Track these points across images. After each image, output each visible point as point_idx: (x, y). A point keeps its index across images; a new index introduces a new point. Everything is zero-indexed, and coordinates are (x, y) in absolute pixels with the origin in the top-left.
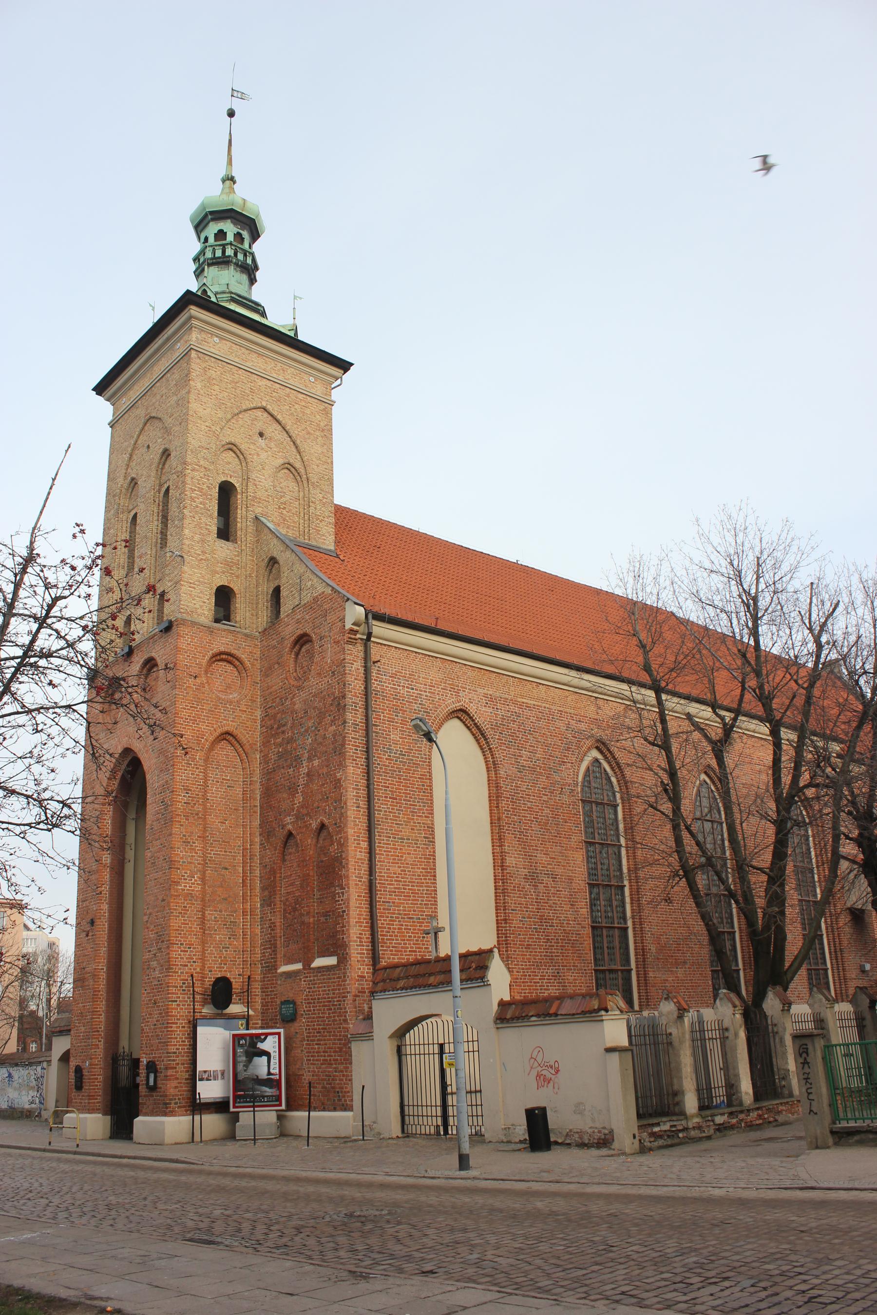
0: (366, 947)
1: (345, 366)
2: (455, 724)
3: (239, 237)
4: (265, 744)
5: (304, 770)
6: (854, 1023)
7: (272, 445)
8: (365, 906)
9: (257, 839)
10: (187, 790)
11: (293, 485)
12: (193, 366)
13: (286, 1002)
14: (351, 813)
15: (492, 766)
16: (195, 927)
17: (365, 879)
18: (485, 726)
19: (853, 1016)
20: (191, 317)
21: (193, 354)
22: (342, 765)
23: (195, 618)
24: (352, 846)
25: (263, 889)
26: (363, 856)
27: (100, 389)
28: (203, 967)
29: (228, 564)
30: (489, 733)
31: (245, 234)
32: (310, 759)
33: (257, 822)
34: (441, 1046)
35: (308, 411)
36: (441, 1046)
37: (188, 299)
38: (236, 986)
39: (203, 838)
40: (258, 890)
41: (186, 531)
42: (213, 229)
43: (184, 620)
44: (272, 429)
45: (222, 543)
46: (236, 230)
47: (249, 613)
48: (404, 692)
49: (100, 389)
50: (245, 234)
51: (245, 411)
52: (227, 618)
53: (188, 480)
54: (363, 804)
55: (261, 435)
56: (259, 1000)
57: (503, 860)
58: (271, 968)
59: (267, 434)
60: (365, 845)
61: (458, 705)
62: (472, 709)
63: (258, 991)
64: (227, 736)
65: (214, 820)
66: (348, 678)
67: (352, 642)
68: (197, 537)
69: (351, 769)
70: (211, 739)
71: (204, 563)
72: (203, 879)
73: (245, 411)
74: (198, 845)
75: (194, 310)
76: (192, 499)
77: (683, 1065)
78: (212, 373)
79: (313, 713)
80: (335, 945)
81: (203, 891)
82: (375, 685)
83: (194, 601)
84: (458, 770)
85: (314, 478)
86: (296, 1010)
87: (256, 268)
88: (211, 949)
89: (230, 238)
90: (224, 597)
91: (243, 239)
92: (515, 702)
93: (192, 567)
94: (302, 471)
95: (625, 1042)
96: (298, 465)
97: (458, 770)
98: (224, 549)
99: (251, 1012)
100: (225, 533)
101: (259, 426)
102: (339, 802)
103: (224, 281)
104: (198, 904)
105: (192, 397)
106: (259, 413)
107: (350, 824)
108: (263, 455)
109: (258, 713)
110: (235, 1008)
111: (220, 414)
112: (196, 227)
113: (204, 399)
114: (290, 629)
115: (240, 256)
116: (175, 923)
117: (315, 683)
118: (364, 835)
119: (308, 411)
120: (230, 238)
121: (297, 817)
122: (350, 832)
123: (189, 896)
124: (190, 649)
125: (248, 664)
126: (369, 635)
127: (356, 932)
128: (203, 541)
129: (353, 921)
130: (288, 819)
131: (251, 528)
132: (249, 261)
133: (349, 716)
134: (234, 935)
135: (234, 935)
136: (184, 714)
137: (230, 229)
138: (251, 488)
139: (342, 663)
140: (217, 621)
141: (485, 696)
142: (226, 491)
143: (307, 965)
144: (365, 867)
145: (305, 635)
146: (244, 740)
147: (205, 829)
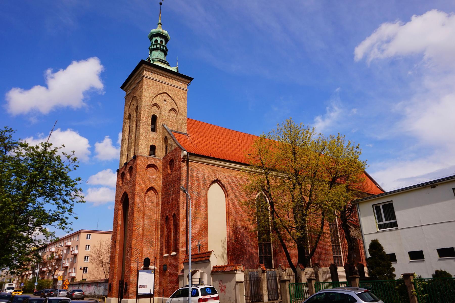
0: (184, 250)
1: (191, 79)
2: (216, 185)
3: (161, 41)
4: (163, 190)
5: (171, 198)
6: (345, 274)
7: (168, 103)
8: (184, 238)
9: (160, 218)
10: (139, 204)
11: (174, 115)
12: (144, 81)
13: (164, 265)
14: (181, 210)
15: (227, 195)
16: (140, 243)
17: (185, 230)
18: (225, 184)
19: (345, 272)
20: (144, 67)
21: (144, 78)
22: (179, 197)
23: (143, 155)
24: (181, 220)
25: (161, 232)
26: (185, 223)
27: (122, 87)
28: (142, 255)
29: (154, 139)
30: (226, 186)
31: (163, 40)
32: (172, 195)
33: (160, 213)
34: (200, 279)
35: (179, 93)
36: (200, 279)
37: (142, 62)
38: (152, 260)
39: (143, 217)
40: (159, 232)
41: (141, 130)
42: (154, 39)
43: (139, 155)
44: (169, 99)
45: (152, 132)
46: (160, 39)
47: (160, 153)
48: (199, 175)
49: (122, 87)
50: (163, 40)
51: (160, 94)
52: (154, 154)
53: (142, 115)
54: (185, 208)
55: (165, 101)
56: (159, 264)
57: (229, 223)
58: (162, 254)
59: (167, 100)
60: (185, 220)
61: (216, 179)
62: (221, 179)
63: (158, 262)
64: (152, 188)
65: (147, 212)
66: (182, 172)
67: (184, 162)
68: (144, 131)
69: (181, 198)
70: (147, 189)
71: (146, 139)
72: (143, 229)
73: (160, 94)
74: (142, 220)
75: (144, 65)
76: (143, 120)
77: (96, 279)
78: (150, 83)
79: (173, 182)
80: (176, 249)
81: (143, 233)
82: (190, 173)
83: (144, 150)
84: (216, 198)
85: (181, 112)
86: (167, 267)
87: (167, 50)
88: (145, 250)
89: (159, 42)
90: (153, 149)
91: (163, 42)
92: (235, 177)
93: (142, 140)
94: (177, 111)
95: (346, 281)
96: (176, 109)
97: (216, 198)
98: (153, 134)
99: (156, 268)
100: (154, 129)
101: (164, 98)
102: (178, 207)
103: (157, 55)
104: (141, 237)
105: (143, 91)
106: (164, 94)
107: (181, 214)
108: (165, 107)
109: (161, 181)
110: (151, 267)
111: (152, 95)
112: (150, 39)
113: (147, 91)
114: (169, 157)
115: (162, 47)
116: (134, 242)
117: (175, 173)
118: (185, 217)
119: (179, 93)
120: (159, 42)
121: (169, 211)
122: (181, 216)
123: (138, 234)
124: (141, 164)
125: (158, 167)
126: (188, 159)
127: (181, 245)
128: (146, 132)
129: (180, 242)
130: (167, 212)
131: (162, 128)
132: (164, 48)
133: (182, 183)
134: (152, 245)
135: (152, 245)
136: (139, 182)
137: (159, 39)
138: (161, 116)
139: (180, 168)
140: (150, 155)
141: (225, 175)
142: (154, 118)
143: (170, 254)
144: (185, 226)
145: (172, 159)
146: (157, 189)
147: (144, 215)
